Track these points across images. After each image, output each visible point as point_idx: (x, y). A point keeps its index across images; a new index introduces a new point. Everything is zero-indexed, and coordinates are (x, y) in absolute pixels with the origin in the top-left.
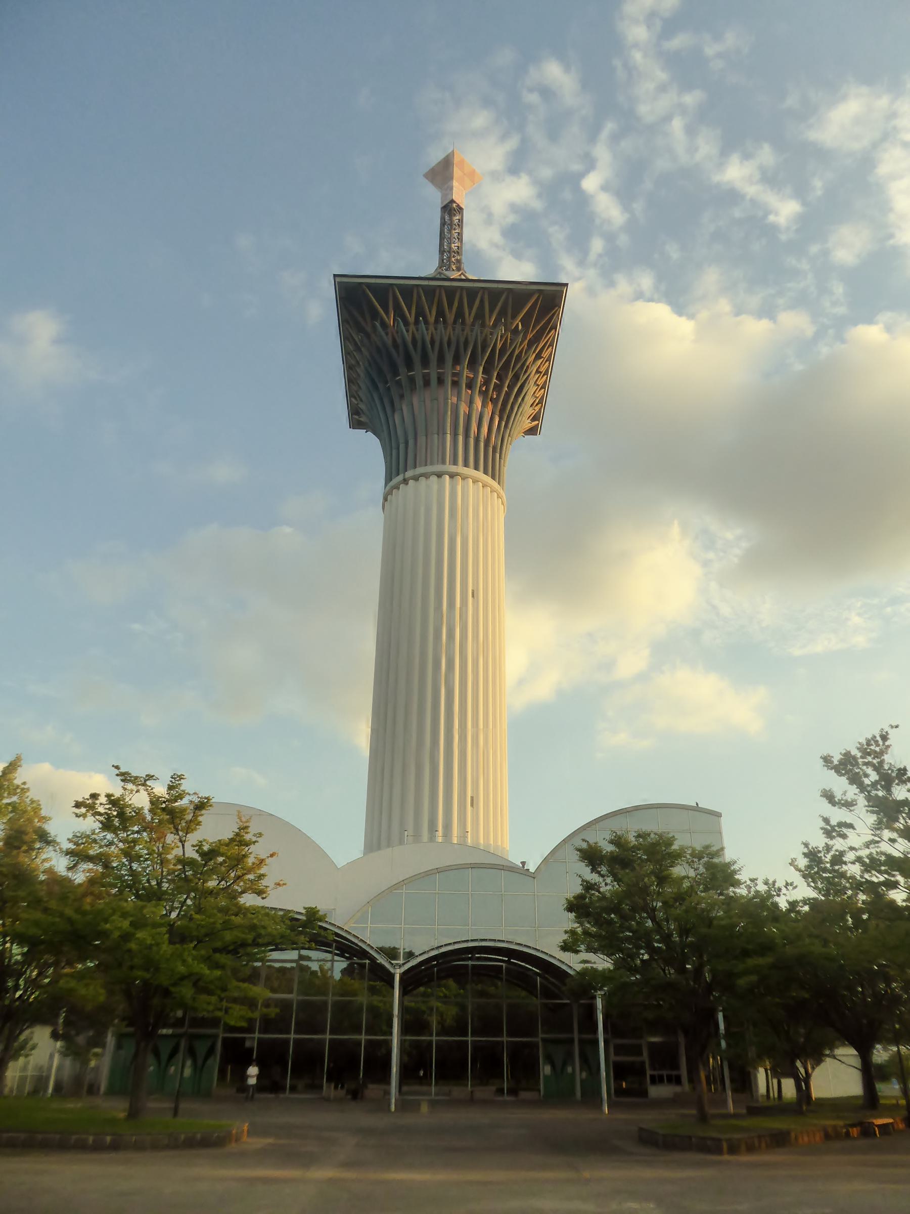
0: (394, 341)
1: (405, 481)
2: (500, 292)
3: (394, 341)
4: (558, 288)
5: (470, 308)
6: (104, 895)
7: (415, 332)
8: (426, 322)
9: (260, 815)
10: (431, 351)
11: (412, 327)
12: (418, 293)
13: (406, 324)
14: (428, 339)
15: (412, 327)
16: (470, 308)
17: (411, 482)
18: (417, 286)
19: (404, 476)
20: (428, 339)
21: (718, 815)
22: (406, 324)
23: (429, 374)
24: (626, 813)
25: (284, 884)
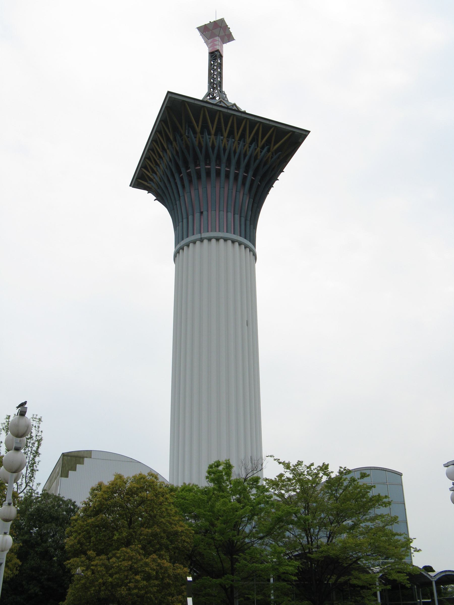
0: (200, 143)
1: (202, 240)
2: (271, 127)
3: (200, 143)
4: (304, 133)
5: (250, 133)
6: (275, 506)
7: (214, 140)
8: (209, 134)
9: (131, 462)
10: (212, 153)
11: (199, 135)
12: (220, 116)
13: (195, 132)
14: (196, 144)
15: (199, 135)
16: (250, 133)
17: (206, 241)
18: (220, 111)
19: (201, 235)
20: (196, 144)
21: (401, 475)
22: (195, 132)
23: (220, 170)
24: (370, 469)
25: (389, 503)
